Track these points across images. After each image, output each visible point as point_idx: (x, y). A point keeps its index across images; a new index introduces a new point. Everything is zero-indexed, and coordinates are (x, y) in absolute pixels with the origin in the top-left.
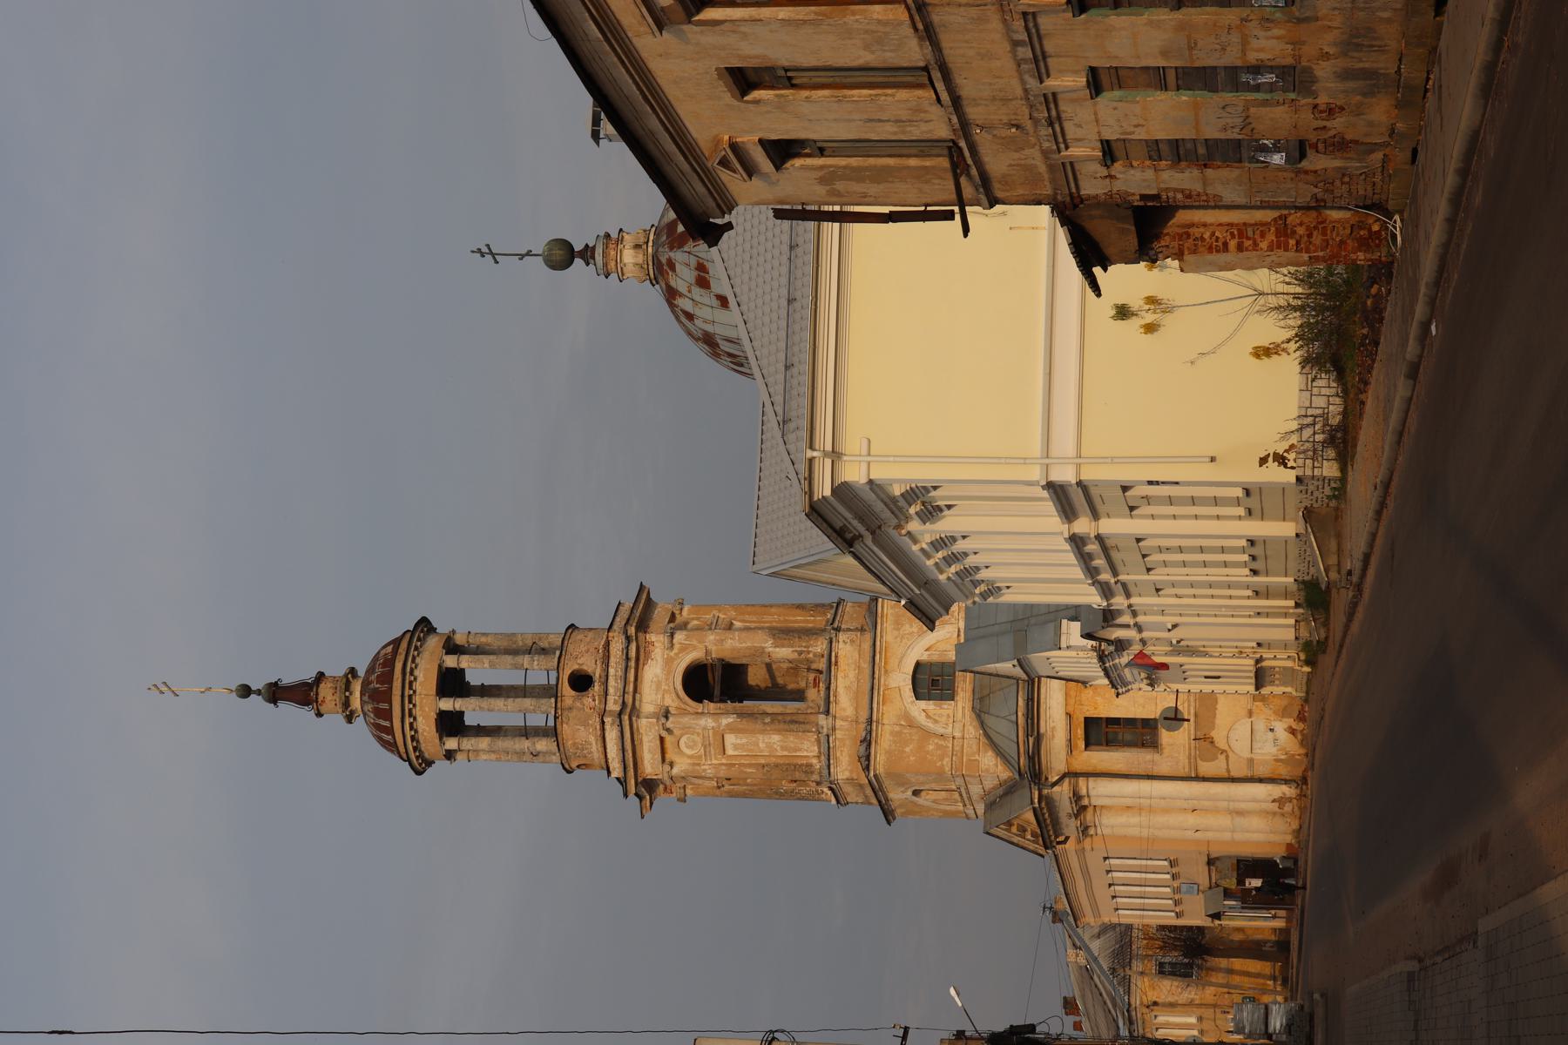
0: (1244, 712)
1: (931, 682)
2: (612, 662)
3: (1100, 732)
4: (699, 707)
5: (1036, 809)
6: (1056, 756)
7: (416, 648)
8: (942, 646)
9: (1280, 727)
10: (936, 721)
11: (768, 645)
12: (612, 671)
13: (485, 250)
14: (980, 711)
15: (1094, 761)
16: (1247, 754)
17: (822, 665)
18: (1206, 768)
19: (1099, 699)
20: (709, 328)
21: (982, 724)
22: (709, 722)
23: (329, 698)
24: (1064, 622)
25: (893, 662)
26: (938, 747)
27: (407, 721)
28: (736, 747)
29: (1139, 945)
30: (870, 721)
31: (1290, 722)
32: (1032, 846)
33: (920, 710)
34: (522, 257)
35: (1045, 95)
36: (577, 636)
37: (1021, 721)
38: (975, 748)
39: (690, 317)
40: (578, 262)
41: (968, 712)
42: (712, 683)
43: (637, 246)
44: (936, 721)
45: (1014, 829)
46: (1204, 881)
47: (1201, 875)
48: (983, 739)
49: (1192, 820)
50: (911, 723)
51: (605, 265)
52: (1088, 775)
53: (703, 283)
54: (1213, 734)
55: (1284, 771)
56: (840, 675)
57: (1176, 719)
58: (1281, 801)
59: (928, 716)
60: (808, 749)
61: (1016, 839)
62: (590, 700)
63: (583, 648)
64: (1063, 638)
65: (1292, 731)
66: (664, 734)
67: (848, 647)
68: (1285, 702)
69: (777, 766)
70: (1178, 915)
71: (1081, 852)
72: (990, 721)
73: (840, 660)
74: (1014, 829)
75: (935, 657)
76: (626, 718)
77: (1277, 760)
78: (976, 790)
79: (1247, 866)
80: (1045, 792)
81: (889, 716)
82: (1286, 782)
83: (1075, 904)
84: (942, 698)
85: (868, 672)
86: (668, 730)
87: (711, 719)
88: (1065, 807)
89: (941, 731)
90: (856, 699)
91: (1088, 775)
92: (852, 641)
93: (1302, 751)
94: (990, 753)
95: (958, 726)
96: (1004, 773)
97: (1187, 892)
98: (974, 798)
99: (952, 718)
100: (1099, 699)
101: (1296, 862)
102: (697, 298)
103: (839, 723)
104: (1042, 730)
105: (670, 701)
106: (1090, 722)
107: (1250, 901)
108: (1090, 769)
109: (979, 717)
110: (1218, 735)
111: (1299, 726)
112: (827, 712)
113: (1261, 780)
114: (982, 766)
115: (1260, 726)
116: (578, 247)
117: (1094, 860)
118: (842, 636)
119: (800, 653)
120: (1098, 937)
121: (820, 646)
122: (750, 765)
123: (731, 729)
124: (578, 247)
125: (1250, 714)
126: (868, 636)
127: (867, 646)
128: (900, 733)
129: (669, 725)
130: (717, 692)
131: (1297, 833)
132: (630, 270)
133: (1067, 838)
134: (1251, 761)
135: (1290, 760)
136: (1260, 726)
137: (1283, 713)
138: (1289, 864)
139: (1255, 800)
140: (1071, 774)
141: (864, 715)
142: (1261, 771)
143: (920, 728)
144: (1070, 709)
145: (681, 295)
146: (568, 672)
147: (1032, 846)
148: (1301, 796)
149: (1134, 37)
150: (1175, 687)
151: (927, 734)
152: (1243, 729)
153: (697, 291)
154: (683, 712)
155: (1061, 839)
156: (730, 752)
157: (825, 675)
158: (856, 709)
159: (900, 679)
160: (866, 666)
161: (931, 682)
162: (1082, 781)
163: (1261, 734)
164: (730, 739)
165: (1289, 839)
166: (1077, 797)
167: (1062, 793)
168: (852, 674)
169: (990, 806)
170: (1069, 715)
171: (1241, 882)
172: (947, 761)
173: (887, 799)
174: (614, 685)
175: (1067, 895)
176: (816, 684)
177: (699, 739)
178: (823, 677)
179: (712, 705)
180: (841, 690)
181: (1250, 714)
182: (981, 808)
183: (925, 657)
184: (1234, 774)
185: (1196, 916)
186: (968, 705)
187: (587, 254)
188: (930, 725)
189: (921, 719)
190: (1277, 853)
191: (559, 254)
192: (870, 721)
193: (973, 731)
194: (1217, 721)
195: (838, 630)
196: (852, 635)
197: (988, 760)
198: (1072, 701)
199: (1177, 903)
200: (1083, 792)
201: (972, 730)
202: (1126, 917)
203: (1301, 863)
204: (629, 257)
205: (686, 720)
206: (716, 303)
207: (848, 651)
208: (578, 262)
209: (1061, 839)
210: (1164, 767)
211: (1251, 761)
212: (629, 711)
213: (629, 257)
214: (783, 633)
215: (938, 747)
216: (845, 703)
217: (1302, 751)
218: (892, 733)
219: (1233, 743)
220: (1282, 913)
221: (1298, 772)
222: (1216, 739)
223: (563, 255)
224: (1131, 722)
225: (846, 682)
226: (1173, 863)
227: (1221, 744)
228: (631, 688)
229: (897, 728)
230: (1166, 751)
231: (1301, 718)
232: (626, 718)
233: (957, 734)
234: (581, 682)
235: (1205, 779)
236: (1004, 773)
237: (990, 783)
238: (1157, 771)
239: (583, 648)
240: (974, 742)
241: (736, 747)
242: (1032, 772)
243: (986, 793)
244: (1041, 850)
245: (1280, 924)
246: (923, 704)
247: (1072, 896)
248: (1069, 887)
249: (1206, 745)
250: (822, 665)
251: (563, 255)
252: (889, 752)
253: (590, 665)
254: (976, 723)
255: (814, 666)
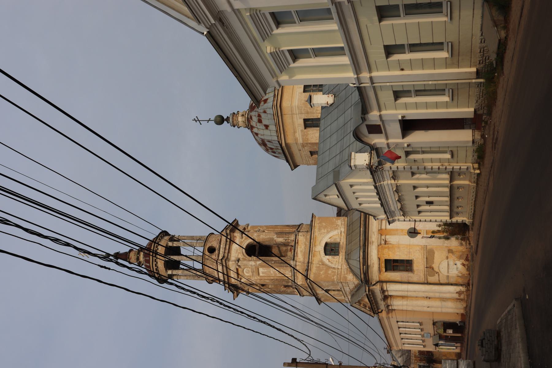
0: (445, 257)
1: (331, 249)
2: (222, 243)
3: (392, 265)
4: (250, 258)
5: (371, 299)
6: (375, 274)
7: (160, 239)
8: (335, 237)
9: (459, 263)
10: (332, 263)
11: (275, 237)
12: (221, 246)
13: (196, 119)
14: (347, 260)
15: (389, 276)
16: (446, 274)
17: (293, 244)
18: (431, 279)
19: (390, 253)
20: (262, 137)
21: (348, 264)
22: (253, 263)
23: (133, 257)
24: (353, 153)
25: (317, 243)
26: (333, 272)
27: (154, 263)
28: (263, 273)
29: (413, 358)
30: (308, 262)
31: (462, 261)
32: (369, 313)
33: (326, 259)
34: (208, 121)
35: (404, 212)
36: (213, 236)
37: (361, 260)
38: (346, 272)
39: (257, 134)
40: (225, 122)
41: (344, 260)
42: (258, 250)
43: (243, 115)
44: (332, 263)
45: (362, 305)
46: (432, 332)
47: (430, 329)
48: (349, 269)
49: (426, 303)
50: (323, 264)
51: (233, 122)
52: (387, 282)
53: (260, 121)
54: (433, 266)
55: (460, 281)
56: (299, 247)
57: (414, 233)
58: (459, 293)
59: (329, 261)
60: (288, 273)
61: (363, 309)
62: (214, 256)
63: (214, 239)
64: (352, 161)
65: (464, 265)
66: (238, 267)
67: (302, 237)
68: (460, 254)
69: (277, 280)
70: (424, 346)
71: (388, 318)
72: (351, 262)
73: (299, 242)
74: (362, 305)
75: (332, 241)
76: (224, 261)
77: (458, 276)
78: (347, 289)
79: (447, 325)
80: (371, 288)
81: (315, 261)
82: (462, 285)
83: (389, 341)
84: (335, 255)
85: (308, 246)
86: (239, 266)
87: (254, 262)
88: (379, 296)
89: (333, 266)
90: (304, 255)
91: (387, 282)
92: (304, 235)
93: (468, 273)
94: (351, 274)
95: (340, 264)
96: (356, 282)
97: (427, 337)
98: (348, 293)
99: (337, 262)
100: (390, 253)
101: (464, 323)
102: (259, 127)
103: (298, 263)
104: (369, 264)
105: (240, 256)
106: (387, 261)
107: (448, 339)
108: (387, 280)
109: (347, 261)
110: (435, 266)
111: (466, 263)
112: (294, 260)
113: (452, 284)
114: (348, 279)
115: (451, 263)
116: (225, 118)
117: (393, 321)
118: (300, 234)
119: (286, 240)
120: (400, 357)
121: (292, 238)
122: (268, 279)
123: (262, 266)
124: (225, 118)
125: (447, 258)
126: (309, 233)
127: (309, 237)
128: (319, 267)
129: (239, 264)
130: (257, 253)
131: (466, 308)
132: (241, 124)
133: (382, 310)
134: (448, 276)
135: (463, 276)
136: (451, 263)
137: (460, 258)
138: (462, 324)
139: (449, 293)
140: (381, 282)
141: (306, 261)
142: (452, 281)
143: (326, 265)
144: (379, 256)
145: (254, 127)
146: (207, 247)
147: (369, 313)
148: (468, 290)
149: (402, 28)
150: (414, 218)
151: (329, 267)
152: (444, 264)
153: (258, 124)
154: (244, 259)
155: (380, 311)
156: (261, 274)
157: (294, 248)
158: (304, 259)
159: (320, 248)
160: (308, 244)
161: (331, 249)
162: (384, 285)
163: (450, 262)
164: (261, 270)
165: (462, 311)
166: (383, 291)
167: (377, 289)
168: (303, 247)
169: (352, 296)
170: (379, 259)
171: (445, 331)
172: (335, 277)
173: (317, 294)
174: (222, 250)
175: (386, 337)
176: (291, 250)
177: (250, 270)
178: (293, 248)
179: (255, 258)
180: (299, 252)
181: (447, 258)
182: (350, 297)
183: (329, 241)
184: (442, 282)
185: (430, 348)
186: (344, 257)
187: (228, 119)
188: (330, 264)
189: (327, 262)
190: (457, 319)
191: (219, 119)
192: (308, 262)
193: (345, 266)
194: (435, 261)
195: (299, 231)
196: (304, 233)
197: (350, 277)
198: (380, 253)
199: (423, 341)
200: (385, 289)
201: (345, 266)
202: (407, 347)
203: (467, 323)
204: (240, 119)
205: (245, 262)
206: (264, 128)
207: (302, 239)
208: (225, 122)
209: (380, 311)
210: (415, 278)
211: (448, 276)
212: (226, 258)
213: (240, 119)
214: (280, 234)
215: (333, 272)
216: (300, 256)
217: (468, 273)
218: (316, 267)
219: (441, 269)
220: (459, 345)
221: (466, 281)
222: (434, 268)
223: (220, 120)
224: (402, 261)
225: (301, 249)
226: (421, 324)
227: (436, 269)
228: (227, 251)
229: (318, 265)
230: (416, 273)
231: (467, 259)
232: (224, 261)
233: (340, 267)
234: (212, 250)
235: (430, 284)
236: (356, 282)
237: (352, 286)
238: (411, 280)
239: (214, 239)
240: (346, 270)
241: (263, 273)
242: (366, 280)
243: (351, 291)
244: (372, 314)
245: (458, 350)
246: (327, 257)
247: (388, 338)
248: (386, 334)
249: (431, 270)
250: (293, 244)
251: (220, 120)
252: (315, 274)
253: (215, 244)
254: (346, 263)
255: (290, 244)
